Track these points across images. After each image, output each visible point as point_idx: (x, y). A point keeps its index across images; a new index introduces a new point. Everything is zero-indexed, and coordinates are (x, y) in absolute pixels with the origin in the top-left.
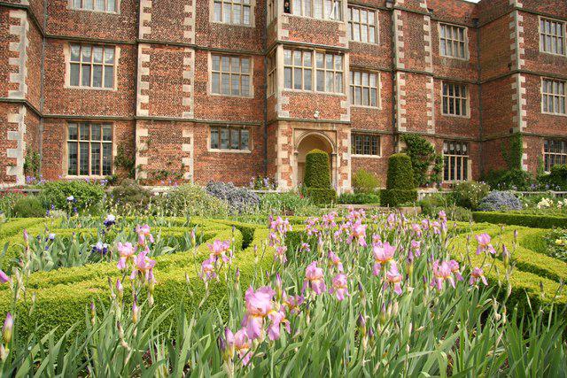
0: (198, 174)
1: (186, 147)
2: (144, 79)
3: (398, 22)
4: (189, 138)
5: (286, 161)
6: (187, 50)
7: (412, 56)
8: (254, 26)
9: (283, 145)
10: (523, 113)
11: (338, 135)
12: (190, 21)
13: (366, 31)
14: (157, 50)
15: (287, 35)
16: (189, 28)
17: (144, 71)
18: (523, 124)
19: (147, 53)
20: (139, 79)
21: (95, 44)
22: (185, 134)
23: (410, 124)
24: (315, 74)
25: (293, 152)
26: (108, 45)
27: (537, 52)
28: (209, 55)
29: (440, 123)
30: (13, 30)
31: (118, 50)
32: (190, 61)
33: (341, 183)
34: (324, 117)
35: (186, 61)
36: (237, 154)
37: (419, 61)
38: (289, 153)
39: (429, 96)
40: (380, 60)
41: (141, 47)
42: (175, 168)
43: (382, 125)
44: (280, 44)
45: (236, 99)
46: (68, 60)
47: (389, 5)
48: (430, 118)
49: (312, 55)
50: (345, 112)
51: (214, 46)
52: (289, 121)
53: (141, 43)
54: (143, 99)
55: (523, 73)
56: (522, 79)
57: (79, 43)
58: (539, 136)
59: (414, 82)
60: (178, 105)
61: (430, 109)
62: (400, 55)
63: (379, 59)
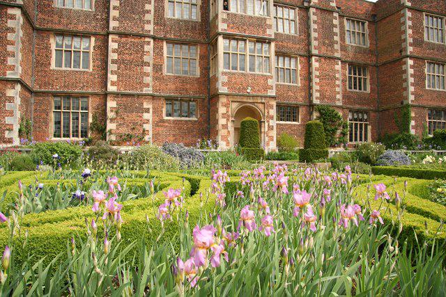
0: (156, 137)
1: (146, 116)
2: (114, 62)
3: (313, 18)
4: (149, 109)
5: (225, 127)
6: (147, 39)
7: (324, 44)
8: (200, 21)
9: (223, 114)
10: (412, 89)
11: (266, 106)
12: (150, 17)
13: (288, 25)
14: (124, 40)
15: (226, 28)
16: (149, 22)
17: (113, 56)
18: (412, 98)
19: (116, 42)
20: (109, 62)
21: (74, 35)
22: (146, 105)
23: (322, 97)
24: (248, 58)
25: (231, 119)
26: (85, 35)
27: (423, 41)
28: (165, 43)
29: (346, 97)
30: (10, 24)
31: (93, 39)
32: (149, 48)
33: (268, 144)
34: (255, 92)
35: (146, 48)
36: (186, 121)
37: (329, 48)
38: (228, 120)
39: (337, 76)
40: (299, 48)
41: (111, 37)
42: (138, 132)
43: (301, 99)
44: (220, 34)
45: (186, 78)
46: (53, 47)
47: (306, 4)
48: (338, 93)
49: (245, 43)
50: (271, 88)
51: (168, 36)
52: (227, 95)
53: (111, 34)
54: (112, 77)
55: (411, 58)
56: (410, 62)
57: (62, 33)
58: (424, 107)
59: (326, 64)
60: (140, 83)
61: (338, 86)
62: (314, 43)
63: (298, 46)
